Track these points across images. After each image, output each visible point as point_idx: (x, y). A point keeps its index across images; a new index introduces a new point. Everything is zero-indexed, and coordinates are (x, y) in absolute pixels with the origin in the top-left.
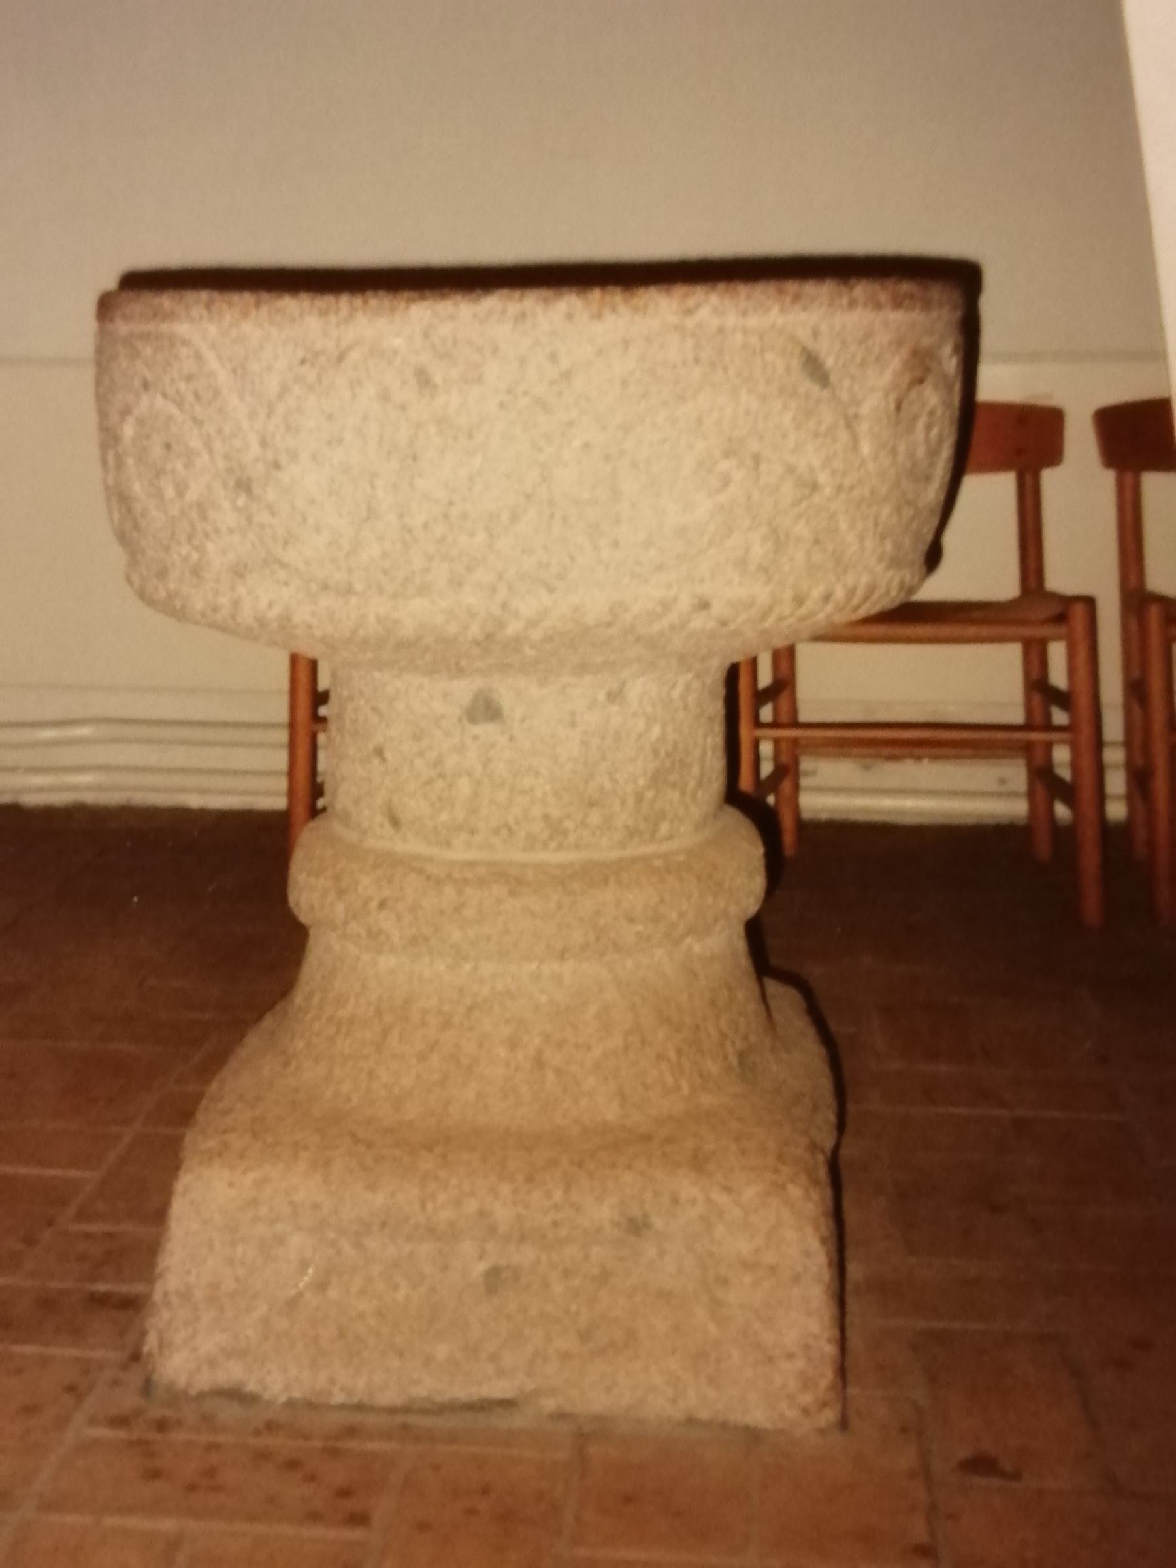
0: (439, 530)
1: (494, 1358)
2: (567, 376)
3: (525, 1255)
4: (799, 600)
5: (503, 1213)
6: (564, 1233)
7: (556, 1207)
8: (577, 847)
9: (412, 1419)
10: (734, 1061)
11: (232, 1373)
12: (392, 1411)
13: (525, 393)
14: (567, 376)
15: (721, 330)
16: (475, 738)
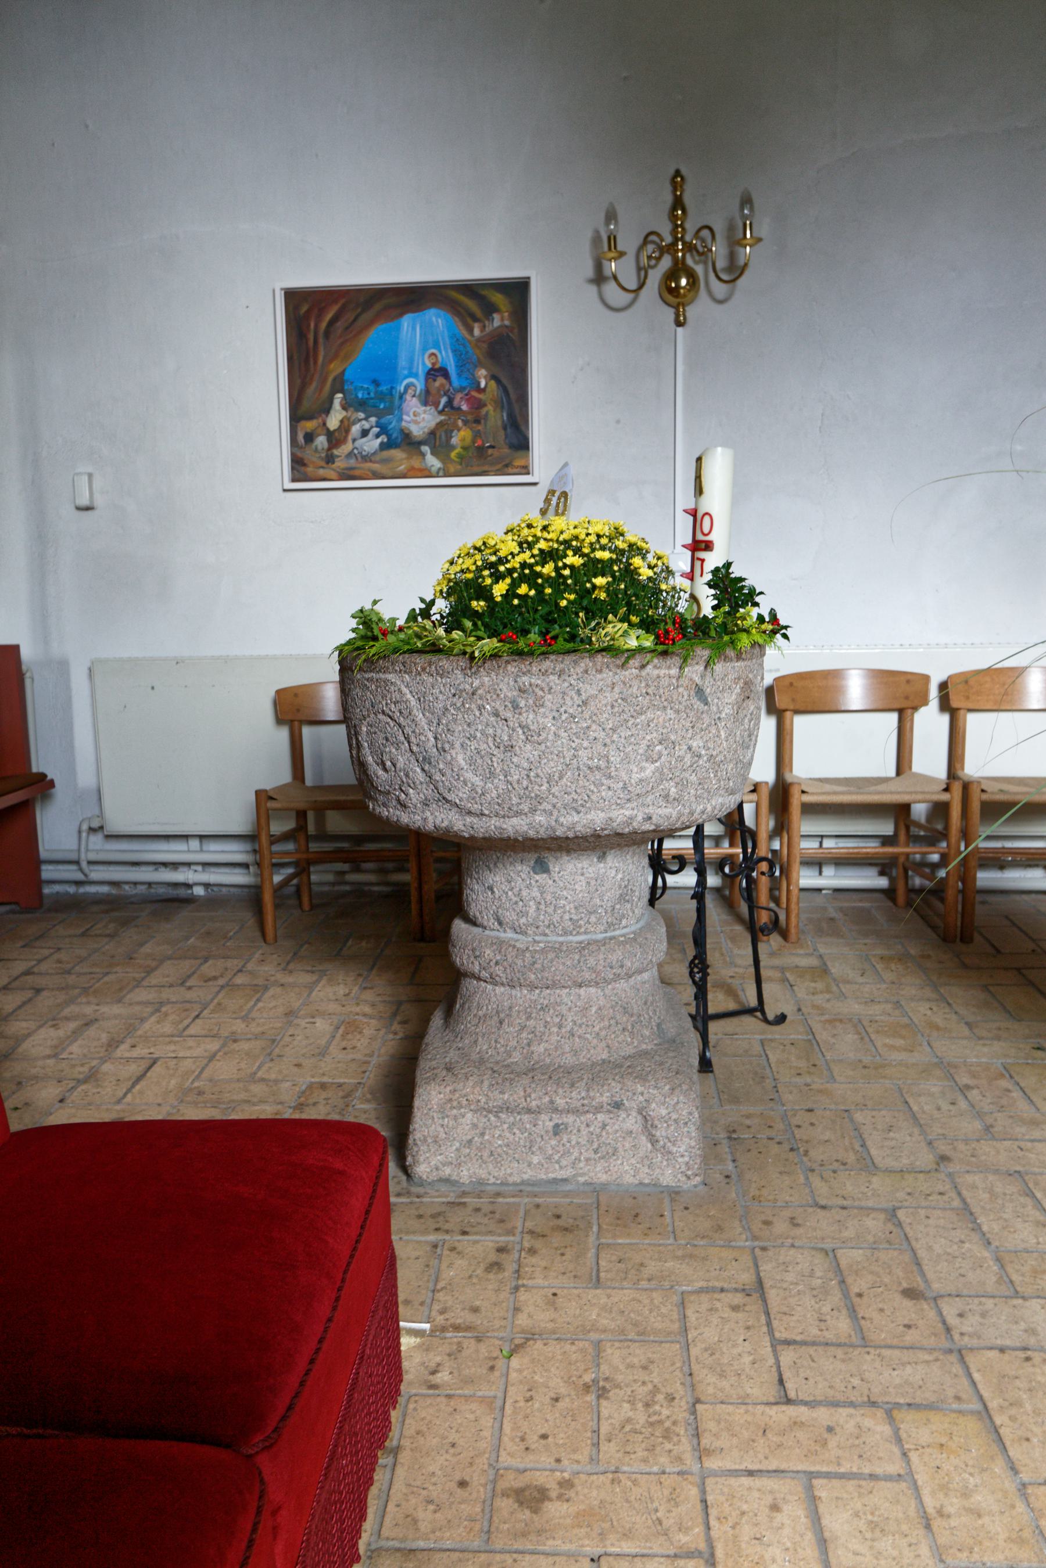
0: (525, 783)
1: (558, 1162)
2: (585, 703)
3: (570, 1119)
5: (560, 1102)
6: (586, 1108)
7: (583, 1098)
8: (585, 933)
9: (522, 1187)
10: (655, 1028)
12: (515, 1184)
14: (585, 703)
15: (659, 677)
16: (537, 881)
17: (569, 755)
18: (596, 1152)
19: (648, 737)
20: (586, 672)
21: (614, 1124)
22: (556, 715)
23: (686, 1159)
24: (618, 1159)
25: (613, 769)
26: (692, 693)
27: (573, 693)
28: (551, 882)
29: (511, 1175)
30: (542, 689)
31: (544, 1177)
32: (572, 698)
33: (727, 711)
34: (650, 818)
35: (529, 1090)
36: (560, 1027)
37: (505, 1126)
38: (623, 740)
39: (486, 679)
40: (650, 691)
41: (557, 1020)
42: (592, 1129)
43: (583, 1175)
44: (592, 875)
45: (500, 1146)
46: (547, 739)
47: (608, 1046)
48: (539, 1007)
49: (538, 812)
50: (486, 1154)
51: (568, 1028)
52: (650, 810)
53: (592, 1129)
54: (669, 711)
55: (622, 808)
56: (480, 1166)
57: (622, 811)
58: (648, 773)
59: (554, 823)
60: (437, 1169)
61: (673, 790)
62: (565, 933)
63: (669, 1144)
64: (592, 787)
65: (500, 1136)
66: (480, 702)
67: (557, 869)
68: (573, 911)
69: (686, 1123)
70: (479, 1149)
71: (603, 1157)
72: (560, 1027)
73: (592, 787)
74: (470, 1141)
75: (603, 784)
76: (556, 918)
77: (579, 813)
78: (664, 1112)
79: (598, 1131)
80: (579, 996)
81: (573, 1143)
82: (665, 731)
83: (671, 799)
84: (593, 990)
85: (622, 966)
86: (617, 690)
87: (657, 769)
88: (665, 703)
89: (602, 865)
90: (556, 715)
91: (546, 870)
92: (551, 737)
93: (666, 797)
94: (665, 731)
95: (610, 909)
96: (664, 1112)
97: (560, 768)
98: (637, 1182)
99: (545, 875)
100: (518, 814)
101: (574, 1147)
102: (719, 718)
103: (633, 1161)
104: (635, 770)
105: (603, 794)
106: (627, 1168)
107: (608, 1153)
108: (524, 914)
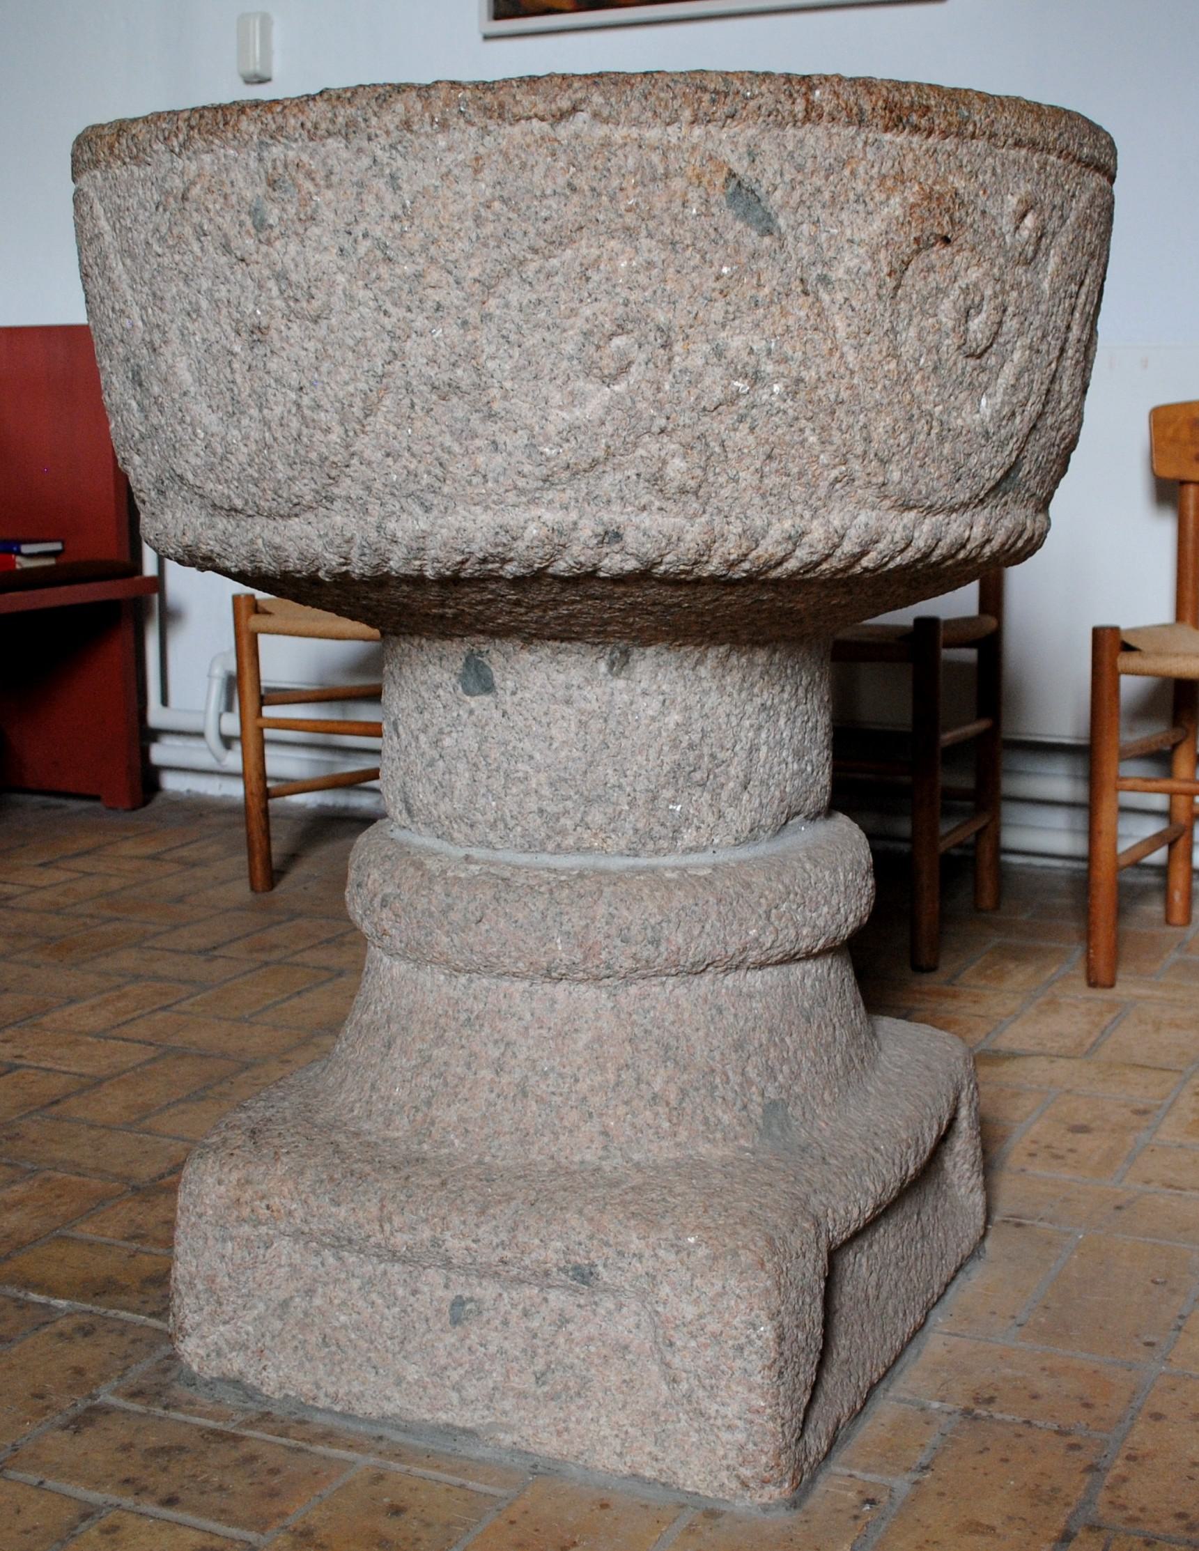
3: (487, 1291)
4: (141, 491)
5: (453, 1244)
11: (236, 1363)
12: (371, 1422)
13: (365, 236)
16: (471, 712)
17: (380, 348)
18: (540, 1379)
19: (587, 311)
20: (407, 125)
21: (587, 1322)
22: (347, 243)
23: (740, 1437)
24: (586, 1407)
25: (495, 392)
26: (718, 196)
27: (380, 184)
28: (497, 715)
29: (360, 1397)
30: (310, 176)
31: (427, 1416)
32: (378, 198)
33: (850, 260)
34: (618, 536)
35: (390, 1207)
36: (499, 1069)
37: (356, 1283)
38: (514, 313)
39: (207, 158)
40: (581, 182)
41: (495, 1053)
42: (535, 1324)
43: (508, 1428)
44: (595, 705)
45: (344, 1327)
46: (328, 307)
47: (605, 1133)
48: (463, 1016)
49: (338, 505)
50: (314, 1338)
51: (517, 1076)
52: (615, 515)
53: (535, 1324)
54: (645, 242)
55: (534, 501)
56: (301, 1365)
57: (535, 512)
58: (592, 409)
59: (373, 535)
60: (219, 1354)
61: (677, 463)
62: (528, 848)
63: (701, 1393)
64: (448, 440)
65: (344, 1303)
66: (196, 218)
67: (510, 684)
68: (546, 791)
69: (741, 1348)
70: (304, 1326)
71: (553, 1397)
72: (499, 1069)
73: (448, 440)
74: (285, 1304)
75: (475, 436)
76: (510, 805)
77: (427, 510)
78: (690, 1312)
79: (548, 1330)
80: (554, 1002)
81: (492, 1349)
82: (635, 296)
83: (671, 489)
84: (587, 993)
85: (656, 942)
86: (487, 175)
87: (617, 401)
88: (630, 219)
89: (621, 684)
90: (347, 243)
91: (488, 687)
92: (338, 303)
93: (656, 481)
94: (635, 296)
95: (641, 799)
96: (690, 1312)
97: (362, 386)
98: (626, 1471)
99: (487, 699)
100: (297, 508)
101: (492, 1358)
102: (824, 279)
103: (621, 1417)
104: (557, 398)
105: (481, 459)
106: (606, 1431)
107: (567, 1388)
108: (444, 790)
